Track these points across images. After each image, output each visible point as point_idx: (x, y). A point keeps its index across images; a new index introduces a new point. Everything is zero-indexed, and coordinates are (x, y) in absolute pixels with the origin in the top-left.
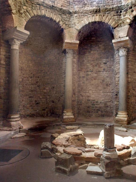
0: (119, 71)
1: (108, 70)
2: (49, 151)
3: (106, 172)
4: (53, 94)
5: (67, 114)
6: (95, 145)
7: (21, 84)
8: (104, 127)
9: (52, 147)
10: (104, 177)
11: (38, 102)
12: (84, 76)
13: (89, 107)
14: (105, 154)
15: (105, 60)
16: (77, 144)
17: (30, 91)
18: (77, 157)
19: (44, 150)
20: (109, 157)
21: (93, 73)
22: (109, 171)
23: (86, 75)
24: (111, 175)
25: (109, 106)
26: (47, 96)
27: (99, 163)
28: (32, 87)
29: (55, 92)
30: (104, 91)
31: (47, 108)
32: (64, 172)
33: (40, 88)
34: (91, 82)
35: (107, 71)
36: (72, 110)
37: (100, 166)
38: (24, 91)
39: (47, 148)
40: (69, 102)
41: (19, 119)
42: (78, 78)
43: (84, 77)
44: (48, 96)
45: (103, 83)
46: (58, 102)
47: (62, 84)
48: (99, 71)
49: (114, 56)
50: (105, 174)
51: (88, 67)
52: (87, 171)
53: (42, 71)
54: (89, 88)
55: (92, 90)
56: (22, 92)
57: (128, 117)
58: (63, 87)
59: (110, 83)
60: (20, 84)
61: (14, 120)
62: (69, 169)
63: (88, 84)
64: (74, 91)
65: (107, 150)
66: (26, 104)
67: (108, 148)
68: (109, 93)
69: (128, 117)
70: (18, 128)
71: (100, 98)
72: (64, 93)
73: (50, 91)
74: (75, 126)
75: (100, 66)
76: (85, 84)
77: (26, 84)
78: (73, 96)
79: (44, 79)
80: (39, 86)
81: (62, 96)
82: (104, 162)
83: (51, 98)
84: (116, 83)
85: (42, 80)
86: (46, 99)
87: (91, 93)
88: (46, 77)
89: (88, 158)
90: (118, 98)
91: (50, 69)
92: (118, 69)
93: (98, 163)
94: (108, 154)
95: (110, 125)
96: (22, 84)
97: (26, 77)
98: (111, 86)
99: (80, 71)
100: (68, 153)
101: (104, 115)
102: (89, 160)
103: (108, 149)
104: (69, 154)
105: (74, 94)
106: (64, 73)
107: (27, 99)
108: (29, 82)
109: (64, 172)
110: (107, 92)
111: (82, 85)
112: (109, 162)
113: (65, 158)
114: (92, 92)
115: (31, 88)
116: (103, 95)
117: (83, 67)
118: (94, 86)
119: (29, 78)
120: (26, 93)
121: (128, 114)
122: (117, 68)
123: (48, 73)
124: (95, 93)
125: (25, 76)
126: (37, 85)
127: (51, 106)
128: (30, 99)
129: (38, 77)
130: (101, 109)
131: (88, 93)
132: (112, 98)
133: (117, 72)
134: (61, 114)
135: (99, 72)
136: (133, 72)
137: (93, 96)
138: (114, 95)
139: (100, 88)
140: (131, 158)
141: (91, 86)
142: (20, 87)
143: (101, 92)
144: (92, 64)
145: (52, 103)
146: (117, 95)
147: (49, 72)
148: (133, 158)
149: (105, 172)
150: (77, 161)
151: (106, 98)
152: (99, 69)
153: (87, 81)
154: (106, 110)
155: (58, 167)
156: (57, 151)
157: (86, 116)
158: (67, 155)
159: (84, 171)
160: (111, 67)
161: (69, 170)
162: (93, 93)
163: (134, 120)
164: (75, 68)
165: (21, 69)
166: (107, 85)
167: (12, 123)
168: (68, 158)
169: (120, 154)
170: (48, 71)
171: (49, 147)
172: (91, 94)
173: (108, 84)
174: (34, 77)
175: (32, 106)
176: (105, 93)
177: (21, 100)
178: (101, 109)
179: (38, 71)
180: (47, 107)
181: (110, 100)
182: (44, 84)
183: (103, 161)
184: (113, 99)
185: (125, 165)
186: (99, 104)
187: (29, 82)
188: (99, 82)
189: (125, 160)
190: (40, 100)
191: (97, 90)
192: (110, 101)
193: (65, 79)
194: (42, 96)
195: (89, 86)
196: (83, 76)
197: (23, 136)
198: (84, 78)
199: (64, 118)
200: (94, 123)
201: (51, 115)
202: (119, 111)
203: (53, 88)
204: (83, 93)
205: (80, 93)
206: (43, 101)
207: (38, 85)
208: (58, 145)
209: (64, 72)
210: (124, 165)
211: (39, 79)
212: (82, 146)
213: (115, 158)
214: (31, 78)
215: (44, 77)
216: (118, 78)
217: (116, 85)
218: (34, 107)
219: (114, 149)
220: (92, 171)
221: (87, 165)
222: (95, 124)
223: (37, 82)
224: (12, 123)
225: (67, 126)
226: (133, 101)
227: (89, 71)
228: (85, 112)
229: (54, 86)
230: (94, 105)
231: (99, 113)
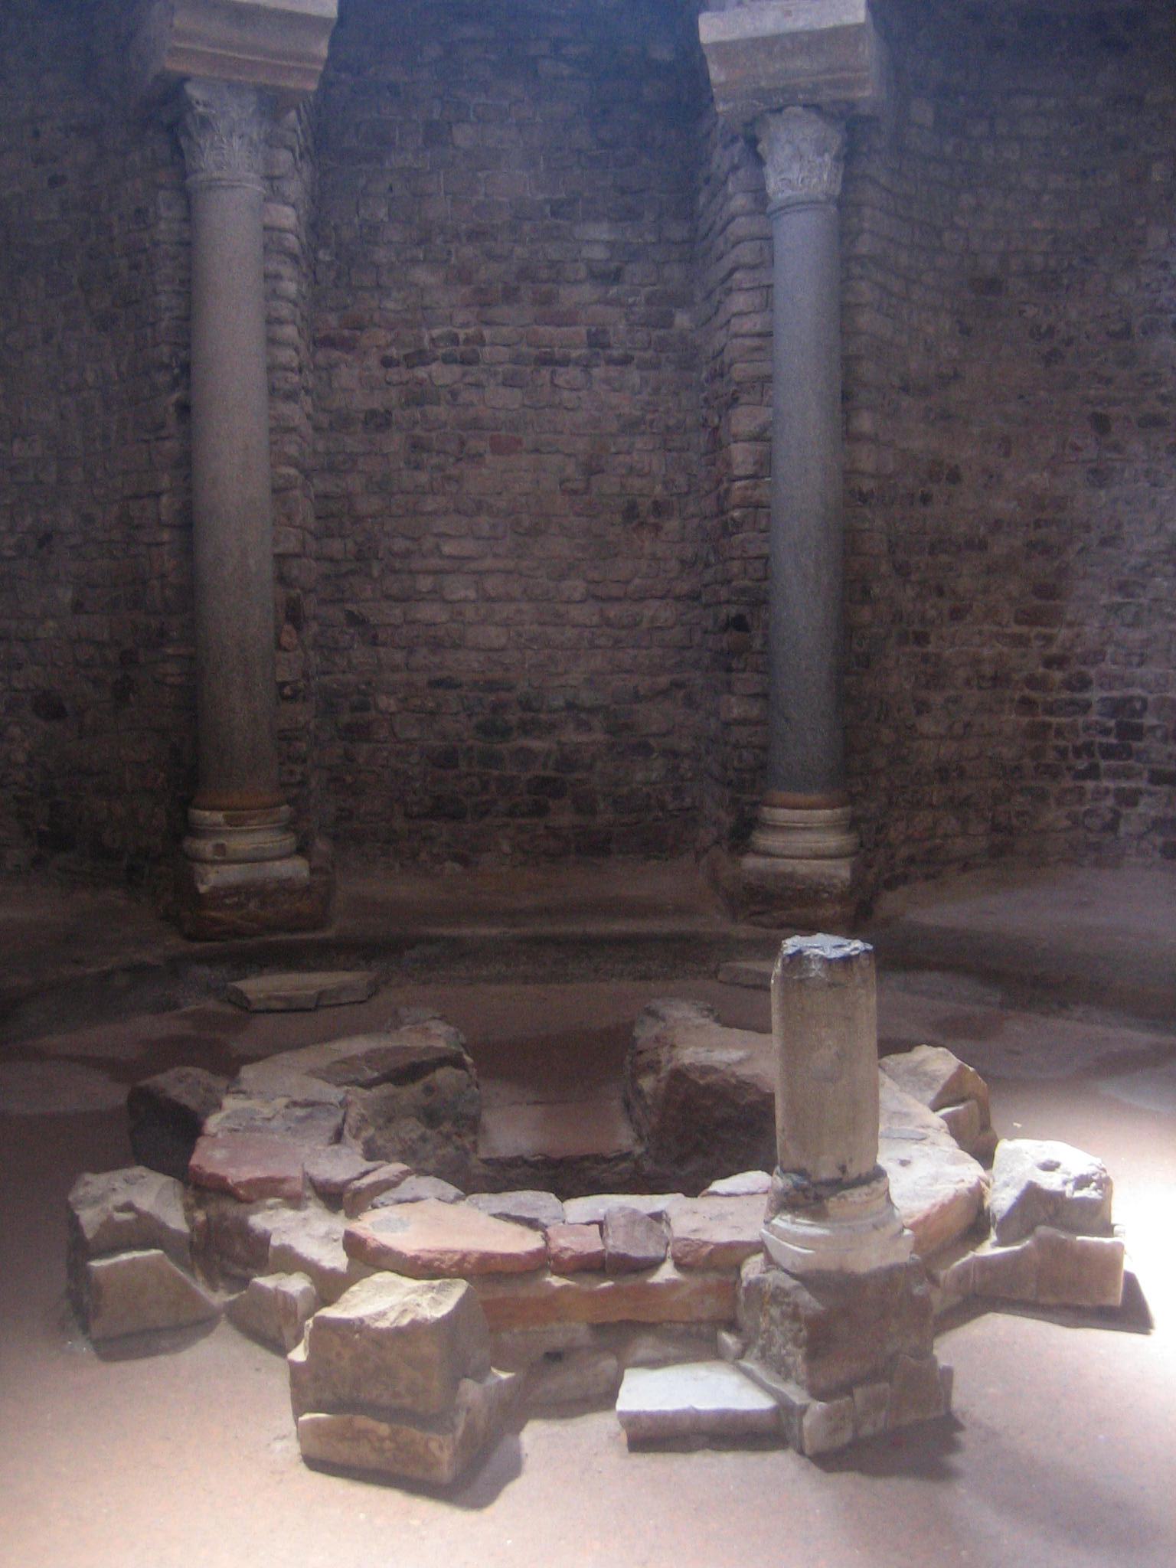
0: (765, 368)
3: (818, 1406)
5: (240, 843)
12: (389, 412)
13: (447, 759)
14: (795, 1239)
15: (601, 231)
19: (124, 1257)
21: (483, 377)
23: (408, 404)
25: (652, 741)
29: (66, 595)
30: (596, 575)
35: (626, 361)
39: (145, 1232)
42: (317, 429)
43: (379, 421)
45: (587, 490)
48: (545, 360)
49: (702, 199)
52: (631, 1421)
54: (447, 548)
55: (473, 566)
57: (855, 853)
59: (658, 488)
63: (430, 504)
68: (658, 603)
69: (855, 853)
72: (189, 593)
74: (332, 968)
75: (548, 299)
83: (20, 667)
84: (736, 496)
87: (465, 600)
98: (672, 525)
99: (336, 354)
102: (626, 1316)
110: (631, 587)
111: (368, 505)
113: (405, 1321)
114: (472, 594)
116: (595, 619)
118: (494, 527)
121: (853, 824)
124: (513, 607)
130: (577, 775)
132: (688, 654)
133: (739, 371)
135: (545, 372)
136: (896, 381)
137: (493, 631)
140: (987, 1244)
143: (575, 587)
144: (463, 276)
146: (739, 624)
149: (804, 1410)
152: (542, 329)
153: (418, 467)
156: (262, 1254)
157: (423, 856)
160: (672, 316)
162: (490, 599)
163: (904, 879)
164: (285, 310)
166: (631, 512)
171: (173, 1225)
172: (469, 612)
173: (645, 506)
176: (611, 599)
178: (577, 775)
181: (663, 680)
192: (664, 693)
195: (441, 525)
196: (372, 414)
198: (379, 428)
199: (203, 889)
200: (526, 931)
202: (780, 796)
203: (45, 539)
205: (350, 607)
216: (757, 438)
222: (541, 941)
225: (244, 977)
227: (440, 352)
228: (408, 816)
230: (505, 733)
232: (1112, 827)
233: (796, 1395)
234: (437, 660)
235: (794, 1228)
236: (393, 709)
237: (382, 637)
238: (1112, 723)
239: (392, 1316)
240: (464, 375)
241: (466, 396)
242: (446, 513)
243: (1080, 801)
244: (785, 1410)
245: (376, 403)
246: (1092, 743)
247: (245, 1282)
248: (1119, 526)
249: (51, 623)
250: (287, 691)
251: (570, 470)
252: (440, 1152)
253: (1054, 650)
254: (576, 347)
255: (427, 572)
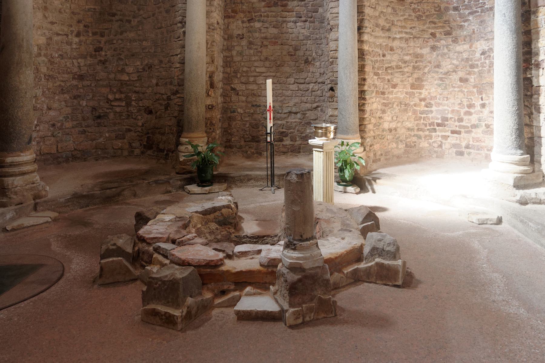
1: (309, 19)
2: (127, 260)
3: (292, 310)
4: (148, 87)
6: (268, 236)
7: (42, 54)
8: (286, 180)
9: (136, 249)
10: (286, 325)
11: (101, 111)
16: (218, 235)
17: (74, 78)
18: (208, 274)
19: (111, 259)
20: (298, 266)
22: (300, 305)
24: (304, 317)
26: (130, 94)
27: (273, 286)
28: (82, 64)
29: (154, 81)
31: (131, 131)
32: (169, 321)
33: (106, 68)
34: (261, 52)
35: (306, 21)
36: (205, 135)
37: (275, 293)
38: (55, 79)
40: (197, 110)
41: (36, 166)
42: (225, 39)
43: (241, 37)
44: (135, 92)
46: (163, 110)
47: (177, 55)
50: (287, 315)
51: (254, 6)
52: (238, 313)
53: (114, 15)
54: (257, 70)
55: (264, 74)
56: (48, 80)
58: (178, 65)
60: (39, 55)
61: (16, 170)
62: (183, 312)
64: (210, 77)
65: (295, 245)
66: (61, 118)
67: (296, 238)
70: (31, 198)
71: (287, 98)
73: (139, 79)
75: (285, 6)
76: (246, 57)
77: (60, 55)
78: (210, 93)
79: (122, 40)
80: (103, 62)
81: (177, 92)
82: (286, 281)
85: (115, 42)
86: (127, 103)
87: (262, 84)
88: (125, 35)
89: (241, 272)
90: (335, 99)
91: (139, 10)
92: (334, 15)
93: (271, 287)
94: (296, 255)
95: (299, 173)
96: (45, 55)
97: (61, 33)
100: (184, 261)
101: (299, 148)
103: (295, 242)
104: (184, 264)
105: (212, 85)
106: (181, 22)
107: (63, 103)
108: (72, 49)
109: (169, 321)
112: (300, 280)
113: (172, 278)
115: (79, 67)
117: (240, 6)
118: (270, 64)
119: (70, 37)
120: (60, 86)
122: (331, 13)
123: (132, 23)
125: (56, 28)
126: (99, 58)
127: (143, 125)
128: (75, 101)
129: (102, 35)
130: (291, 131)
131: (254, 85)
134: (172, 147)
138: (326, 90)
139: (287, 69)
140: (362, 263)
141: (262, 63)
142: (42, 65)
143: (292, 80)
145: (146, 116)
146: (332, 89)
147: (136, 20)
148: (366, 263)
149: (287, 311)
150: (210, 286)
151: (305, 99)
152: (283, 13)
153: (251, 49)
154: (304, 135)
155: (151, 306)
158: (177, 267)
159: (230, 312)
161: (184, 314)
165: (45, 5)
167: (9, 181)
168: (181, 277)
169: (332, 257)
170: (134, 17)
173: (310, 59)
174: (88, 32)
175: (82, 127)
176: (300, 84)
177: (45, 107)
178: (291, 131)
179: (100, 14)
180: (131, 128)
181: (315, 105)
182: (121, 55)
183: (282, 279)
184: (324, 101)
185: (347, 285)
186: (285, 118)
187: (72, 49)
188: (285, 53)
189: (345, 272)
190: (107, 105)
191: (278, 74)
193: (185, 40)
194: (114, 93)
195: (256, 64)
197: (47, 222)
201: (143, 153)
204: (240, 85)
206: (118, 109)
207: (102, 59)
208: (154, 241)
209: (183, 19)
210: (344, 287)
211: (103, 40)
212: (228, 239)
213: (314, 266)
214: (78, 35)
215: (121, 33)
217: (331, 60)
218: (89, 129)
219: (311, 241)
220: (252, 309)
221: (237, 295)
223: (98, 50)
224: (9, 181)
226: (375, 106)
228: (245, 141)
229: (151, 61)
231: (284, 143)
232: (440, 146)
233: (286, 306)
234: (254, 99)
235: (294, 255)
236: (242, 112)
237: (240, 93)
238: (440, 117)
239: (169, 277)
240: (263, 25)
241: (263, 30)
242: (258, 61)
243: (431, 139)
244: (283, 311)
245: (240, 32)
246: (434, 122)
247: (143, 267)
248: (440, 62)
249: (150, 89)
250: (210, 107)
251: (291, 49)
252: (222, 233)
253: (423, 96)
254: (293, 17)
255: (252, 76)
